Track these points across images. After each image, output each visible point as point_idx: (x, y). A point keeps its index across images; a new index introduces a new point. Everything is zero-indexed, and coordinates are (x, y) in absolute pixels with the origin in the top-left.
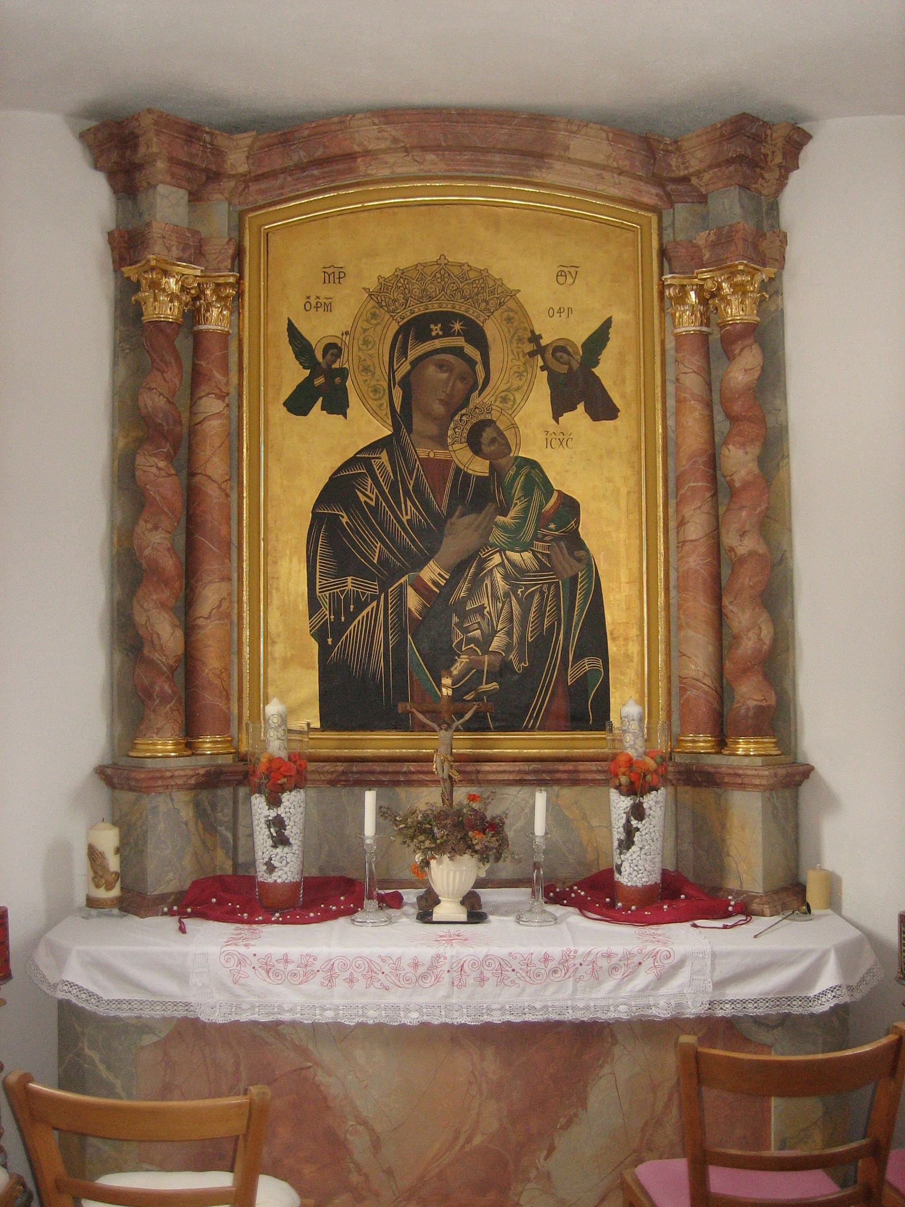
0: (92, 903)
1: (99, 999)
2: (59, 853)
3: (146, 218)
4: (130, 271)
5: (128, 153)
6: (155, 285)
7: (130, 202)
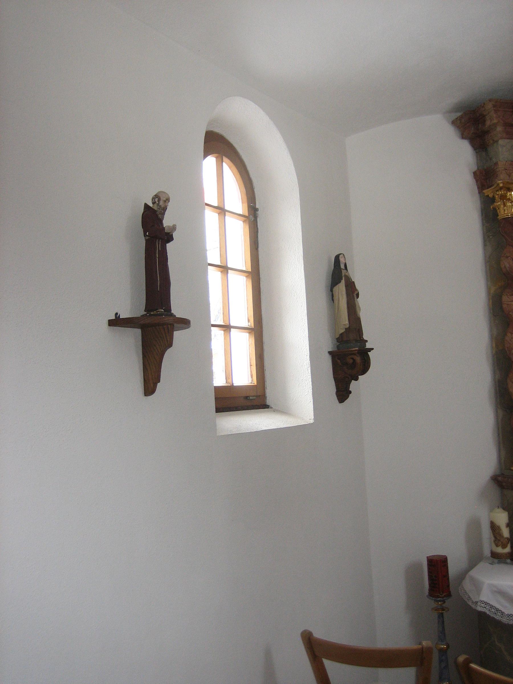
0: (494, 555)
1: (503, 613)
2: (474, 525)
3: (494, 160)
4: (488, 192)
5: (480, 126)
6: (503, 197)
7: (484, 154)
